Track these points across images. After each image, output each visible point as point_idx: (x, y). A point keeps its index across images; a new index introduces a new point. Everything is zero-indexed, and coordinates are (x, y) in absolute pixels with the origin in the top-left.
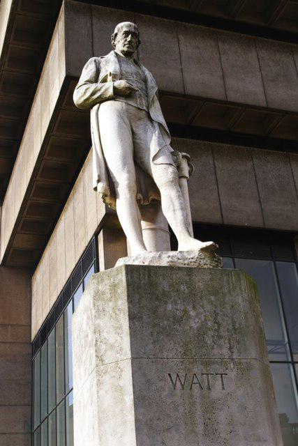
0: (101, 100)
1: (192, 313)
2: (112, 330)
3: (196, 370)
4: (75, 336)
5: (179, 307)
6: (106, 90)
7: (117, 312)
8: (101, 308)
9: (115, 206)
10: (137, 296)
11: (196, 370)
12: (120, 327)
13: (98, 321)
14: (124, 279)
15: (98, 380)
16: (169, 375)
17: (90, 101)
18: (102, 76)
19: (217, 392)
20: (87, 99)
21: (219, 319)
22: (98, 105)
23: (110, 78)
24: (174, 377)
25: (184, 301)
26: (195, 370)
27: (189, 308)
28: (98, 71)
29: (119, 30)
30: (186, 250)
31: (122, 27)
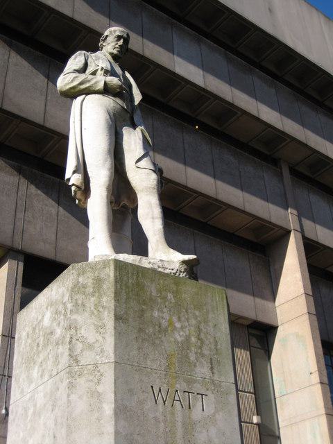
0: (88, 92)
1: (178, 325)
2: (92, 327)
3: (179, 387)
4: (24, 334)
5: (165, 315)
6: (96, 83)
7: (101, 310)
8: (80, 302)
9: (86, 203)
10: (124, 296)
11: (179, 387)
12: (103, 326)
13: (74, 317)
14: (112, 274)
15: (70, 382)
16: (152, 387)
17: (76, 90)
18: (90, 69)
19: (197, 413)
20: (74, 88)
21: (202, 336)
22: (83, 96)
23: (99, 72)
24: (156, 389)
25: (170, 310)
26: (178, 386)
27: (175, 319)
28: (86, 65)
29: (111, 32)
30: (167, 260)
31: (115, 31)
